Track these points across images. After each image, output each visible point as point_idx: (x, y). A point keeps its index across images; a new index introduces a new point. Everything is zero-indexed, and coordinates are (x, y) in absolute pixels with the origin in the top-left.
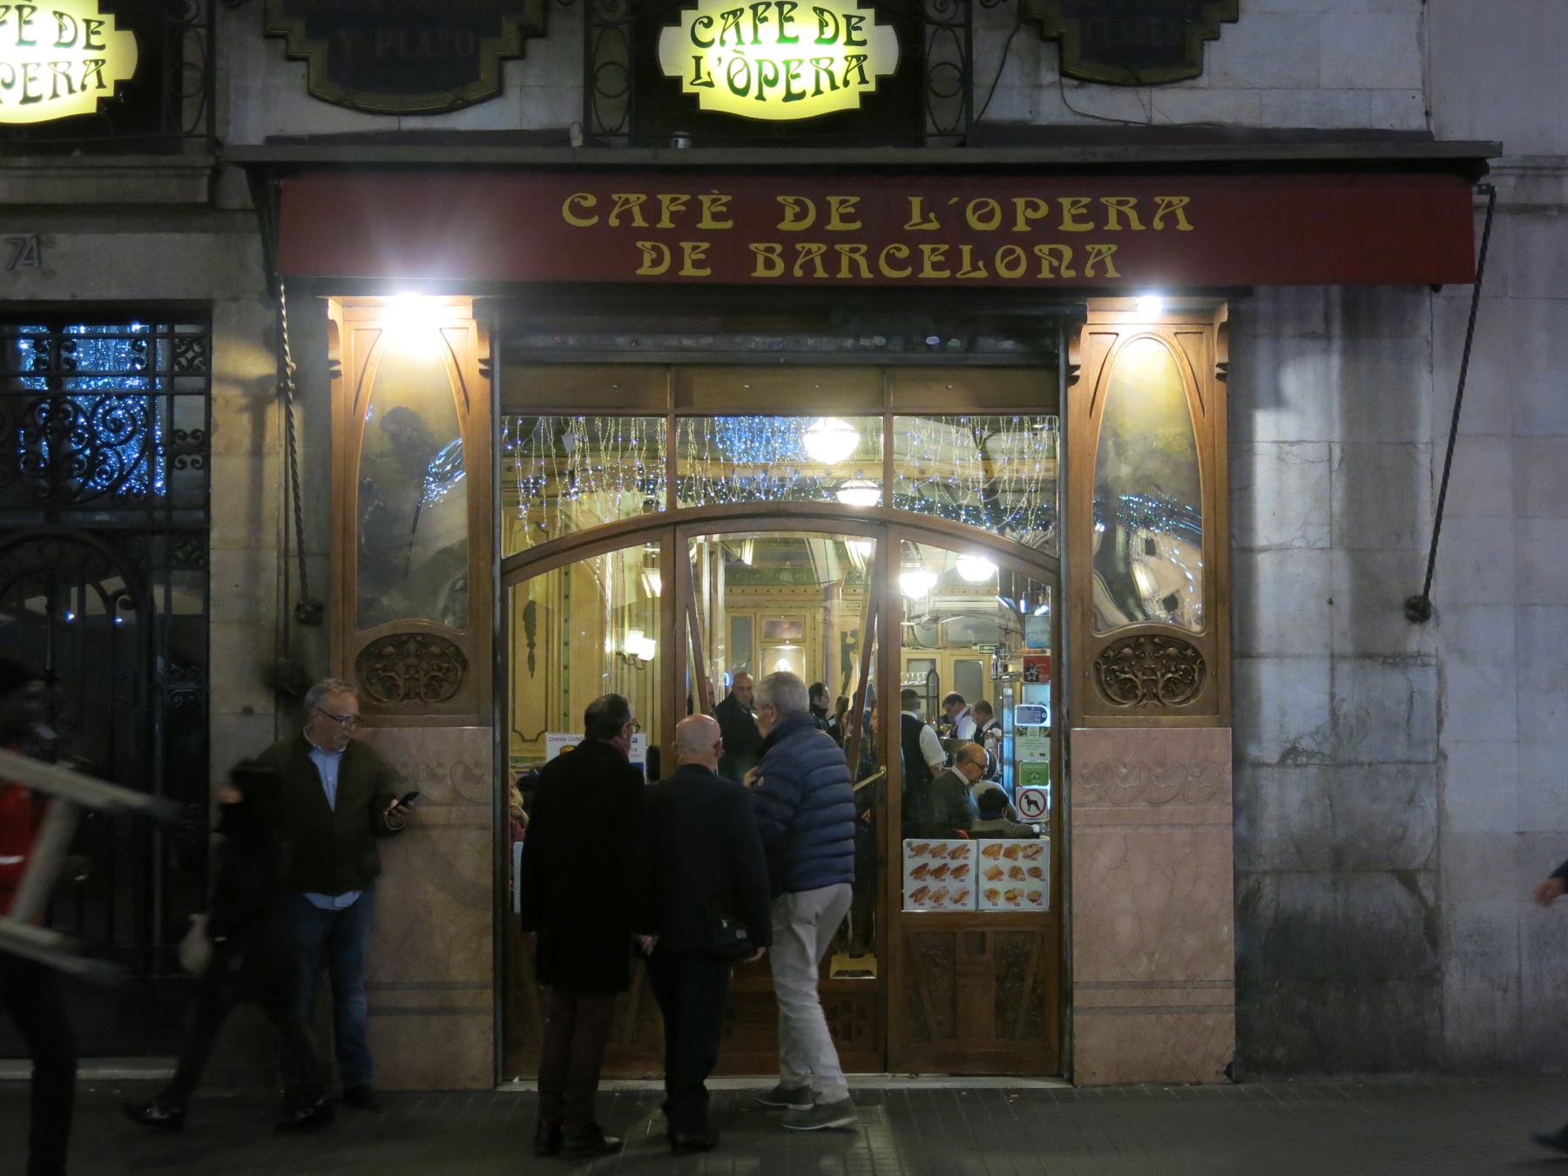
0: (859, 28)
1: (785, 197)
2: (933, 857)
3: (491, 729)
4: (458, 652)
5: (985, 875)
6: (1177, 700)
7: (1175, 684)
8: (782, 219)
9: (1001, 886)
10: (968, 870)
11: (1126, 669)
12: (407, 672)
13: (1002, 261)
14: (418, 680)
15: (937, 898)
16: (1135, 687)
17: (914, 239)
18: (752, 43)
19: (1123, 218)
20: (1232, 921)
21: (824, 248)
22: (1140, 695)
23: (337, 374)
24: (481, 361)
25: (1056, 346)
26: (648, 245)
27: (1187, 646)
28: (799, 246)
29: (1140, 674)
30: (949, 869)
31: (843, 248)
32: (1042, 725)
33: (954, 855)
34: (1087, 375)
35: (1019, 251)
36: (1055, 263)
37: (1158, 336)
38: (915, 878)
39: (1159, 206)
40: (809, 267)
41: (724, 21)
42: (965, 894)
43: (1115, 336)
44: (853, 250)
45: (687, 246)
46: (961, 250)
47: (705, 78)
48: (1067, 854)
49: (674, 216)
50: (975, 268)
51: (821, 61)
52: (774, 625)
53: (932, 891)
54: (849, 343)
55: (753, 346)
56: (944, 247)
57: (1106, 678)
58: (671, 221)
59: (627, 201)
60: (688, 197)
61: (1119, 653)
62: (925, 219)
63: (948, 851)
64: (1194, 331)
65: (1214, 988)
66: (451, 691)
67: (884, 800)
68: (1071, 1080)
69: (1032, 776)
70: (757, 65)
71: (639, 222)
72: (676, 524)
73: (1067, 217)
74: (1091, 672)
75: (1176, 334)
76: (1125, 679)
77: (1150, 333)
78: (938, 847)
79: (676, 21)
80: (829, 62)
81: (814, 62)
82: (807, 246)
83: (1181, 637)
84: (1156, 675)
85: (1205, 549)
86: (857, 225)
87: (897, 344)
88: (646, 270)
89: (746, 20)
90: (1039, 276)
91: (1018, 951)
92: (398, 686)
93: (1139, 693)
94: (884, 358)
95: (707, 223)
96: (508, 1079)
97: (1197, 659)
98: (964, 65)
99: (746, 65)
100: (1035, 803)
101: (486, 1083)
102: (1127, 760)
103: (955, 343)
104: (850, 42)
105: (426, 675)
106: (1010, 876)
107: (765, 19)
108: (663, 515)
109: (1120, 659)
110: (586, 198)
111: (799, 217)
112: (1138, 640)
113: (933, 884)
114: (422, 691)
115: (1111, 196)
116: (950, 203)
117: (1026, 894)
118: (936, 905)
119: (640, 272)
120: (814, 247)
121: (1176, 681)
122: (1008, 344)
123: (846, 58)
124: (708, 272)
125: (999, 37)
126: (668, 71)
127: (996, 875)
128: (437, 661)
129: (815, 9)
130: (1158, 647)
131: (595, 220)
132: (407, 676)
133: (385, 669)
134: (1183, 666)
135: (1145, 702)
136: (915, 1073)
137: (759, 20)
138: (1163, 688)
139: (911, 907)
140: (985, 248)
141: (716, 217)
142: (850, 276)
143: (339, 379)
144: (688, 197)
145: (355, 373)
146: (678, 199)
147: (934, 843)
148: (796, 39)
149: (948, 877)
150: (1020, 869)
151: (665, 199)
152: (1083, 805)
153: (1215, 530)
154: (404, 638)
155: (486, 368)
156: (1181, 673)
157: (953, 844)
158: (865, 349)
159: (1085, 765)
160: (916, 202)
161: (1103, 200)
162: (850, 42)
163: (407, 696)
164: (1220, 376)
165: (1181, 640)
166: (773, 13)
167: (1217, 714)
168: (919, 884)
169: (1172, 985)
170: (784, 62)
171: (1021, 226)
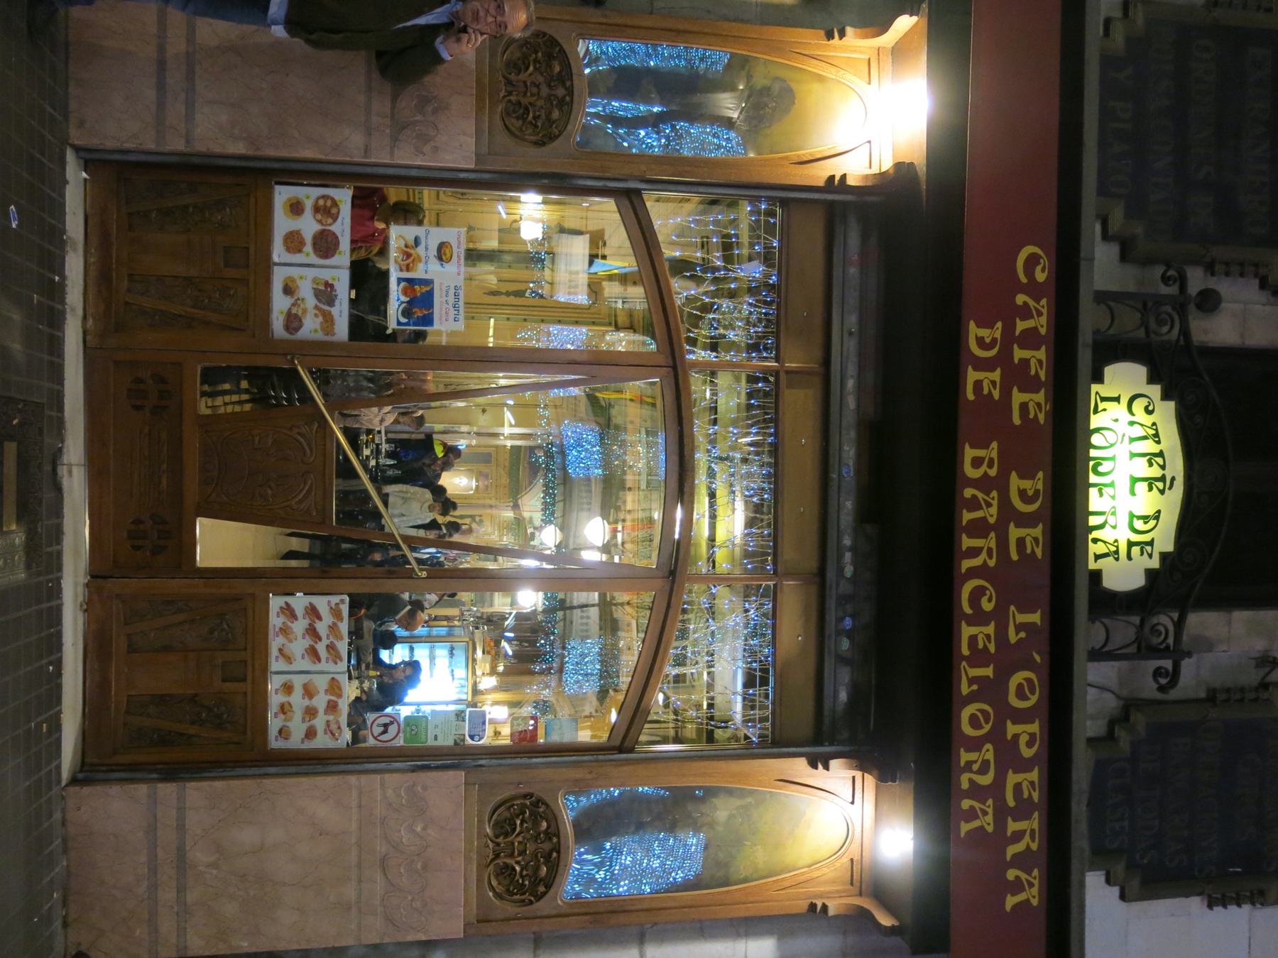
0: (1142, 554)
1: (1041, 480)
2: (330, 626)
3: (472, 166)
4: (553, 138)
5: (311, 680)
6: (494, 883)
7: (510, 875)
8: (1021, 477)
9: (297, 700)
10: (315, 663)
11: (525, 825)
12: (533, 84)
13: (978, 710)
14: (525, 94)
15: (285, 631)
16: (506, 835)
17: (999, 616)
18: (1130, 452)
19: (1018, 836)
20: (253, 950)
21: (992, 520)
22: (497, 840)
23: (830, 36)
24: (844, 177)
25: (840, 743)
26: (998, 335)
27: (548, 887)
28: (994, 494)
29: (520, 839)
30: (316, 643)
31: (992, 541)
32: (467, 738)
33: (331, 648)
34: (818, 776)
35: (987, 728)
36: (975, 767)
37: (851, 843)
38: (307, 607)
39: (1030, 874)
40: (974, 504)
41: (1150, 425)
42: (289, 659)
43: (851, 800)
44: (990, 551)
45: (996, 375)
46: (988, 666)
47: (1101, 406)
48: (329, 768)
49: (1025, 363)
50: (972, 681)
51: (1113, 517)
52: (486, 476)
53: (292, 625)
54: (847, 541)
55: (846, 448)
56: (992, 648)
57: (517, 805)
58: (1020, 360)
59: (1040, 314)
60: (1043, 378)
61: (541, 817)
62: (1019, 628)
63: (335, 642)
64: (855, 877)
65: (178, 935)
66: (513, 129)
67: (391, 575)
68: (74, 781)
69: (413, 728)
70: (1110, 456)
71: (1021, 326)
72: (674, 368)
73: (1019, 777)
74: (524, 789)
75: (852, 860)
76: (515, 824)
77: (853, 835)
78: (340, 632)
79: (1151, 380)
80: (1113, 525)
81: (1113, 510)
82: (995, 503)
83: (557, 880)
84: (519, 855)
85: (332, 440)
86: (1015, 556)
87: (845, 588)
88: (974, 330)
89: (1150, 447)
90: (962, 750)
91: (225, 716)
92: (518, 74)
93: (500, 840)
94: (831, 575)
95: (1018, 397)
96: (87, 165)
97: (535, 897)
98: (1109, 653)
99: (1112, 445)
100: (385, 732)
101: (76, 136)
102: (430, 831)
103: (845, 644)
104: (1131, 544)
105: (530, 104)
106: (307, 707)
107: (1151, 465)
108: (683, 357)
109: (536, 818)
110: (1043, 271)
111: (1022, 494)
112: (555, 835)
113: (300, 626)
114: (513, 98)
115: (1039, 823)
116: (1035, 654)
117: (288, 724)
118: (277, 630)
119: (972, 325)
120: (994, 510)
121: (512, 876)
122: (843, 696)
123: (1116, 541)
124: (971, 396)
125: (1113, 683)
126: (1109, 371)
127: (309, 692)
128: (543, 116)
129: (1159, 512)
130: (548, 857)
131: (1024, 280)
132: (528, 84)
133: (536, 61)
134: (527, 883)
135: (491, 845)
136: (88, 607)
137: (1151, 459)
138: (504, 863)
139: (276, 602)
140: (991, 691)
141: (1024, 407)
142: (964, 549)
143: (825, 38)
144: (1043, 378)
145: (828, 56)
146: (1041, 368)
147: (344, 627)
148: (1133, 493)
149: (307, 642)
150: (314, 718)
151: (1041, 354)
152: (382, 785)
153: (669, 908)
154: (568, 84)
155: (836, 182)
156: (521, 881)
157: (343, 647)
158: (840, 557)
159: (425, 788)
160: (1035, 618)
161: (1036, 815)
162: (1131, 544)
163: (509, 82)
164: (813, 907)
165: (553, 881)
166: (1155, 472)
167: (478, 922)
168: (300, 612)
169: (181, 889)
170: (1113, 482)
171: (1012, 729)
